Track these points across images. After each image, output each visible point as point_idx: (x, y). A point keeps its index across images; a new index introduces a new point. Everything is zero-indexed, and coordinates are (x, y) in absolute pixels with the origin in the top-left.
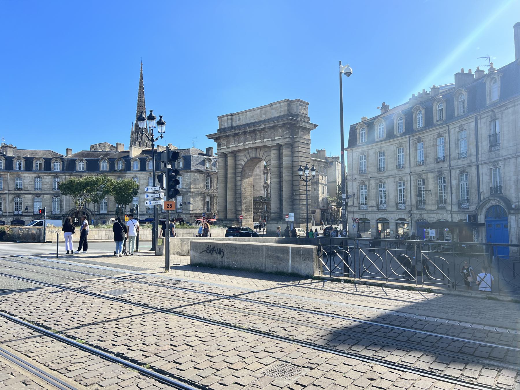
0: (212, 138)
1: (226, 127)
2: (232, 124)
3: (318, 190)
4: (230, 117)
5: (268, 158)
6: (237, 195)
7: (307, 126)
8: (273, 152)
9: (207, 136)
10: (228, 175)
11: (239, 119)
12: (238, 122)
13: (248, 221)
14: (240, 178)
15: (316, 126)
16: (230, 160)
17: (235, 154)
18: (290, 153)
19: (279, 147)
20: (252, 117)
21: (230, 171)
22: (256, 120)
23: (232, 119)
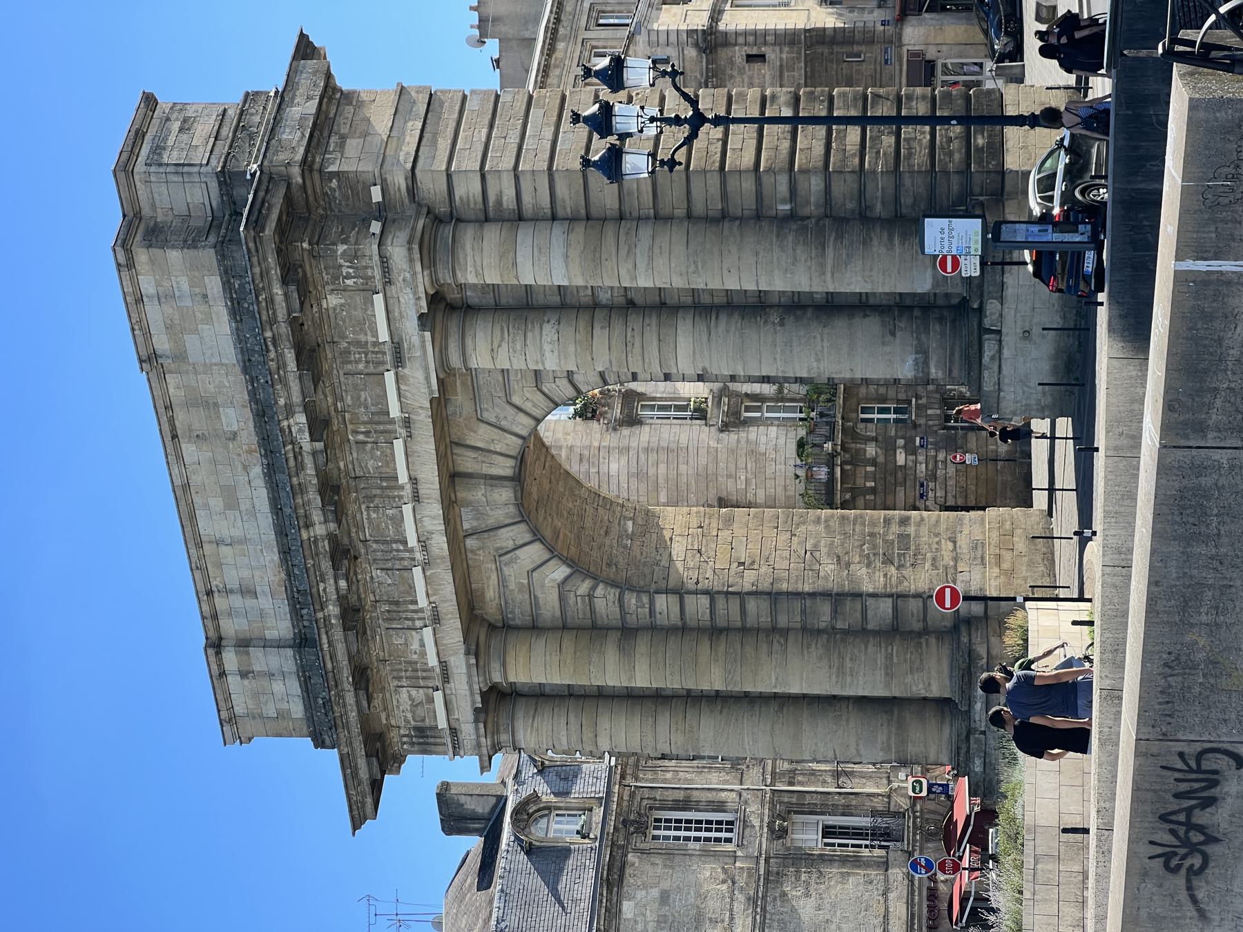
0: (376, 786)
1: (295, 687)
2: (279, 645)
3: (759, 36)
4: (230, 658)
5: (526, 396)
6: (783, 621)
7: (304, 108)
8: (480, 358)
9: (356, 824)
10: (642, 679)
11: (248, 591)
12: (265, 602)
13: (975, 546)
14: (661, 601)
15: (305, 49)
16: (532, 666)
17: (486, 628)
18: (492, 234)
19: (447, 309)
20: (231, 502)
21: (610, 672)
22: (257, 470)
23: (244, 644)
